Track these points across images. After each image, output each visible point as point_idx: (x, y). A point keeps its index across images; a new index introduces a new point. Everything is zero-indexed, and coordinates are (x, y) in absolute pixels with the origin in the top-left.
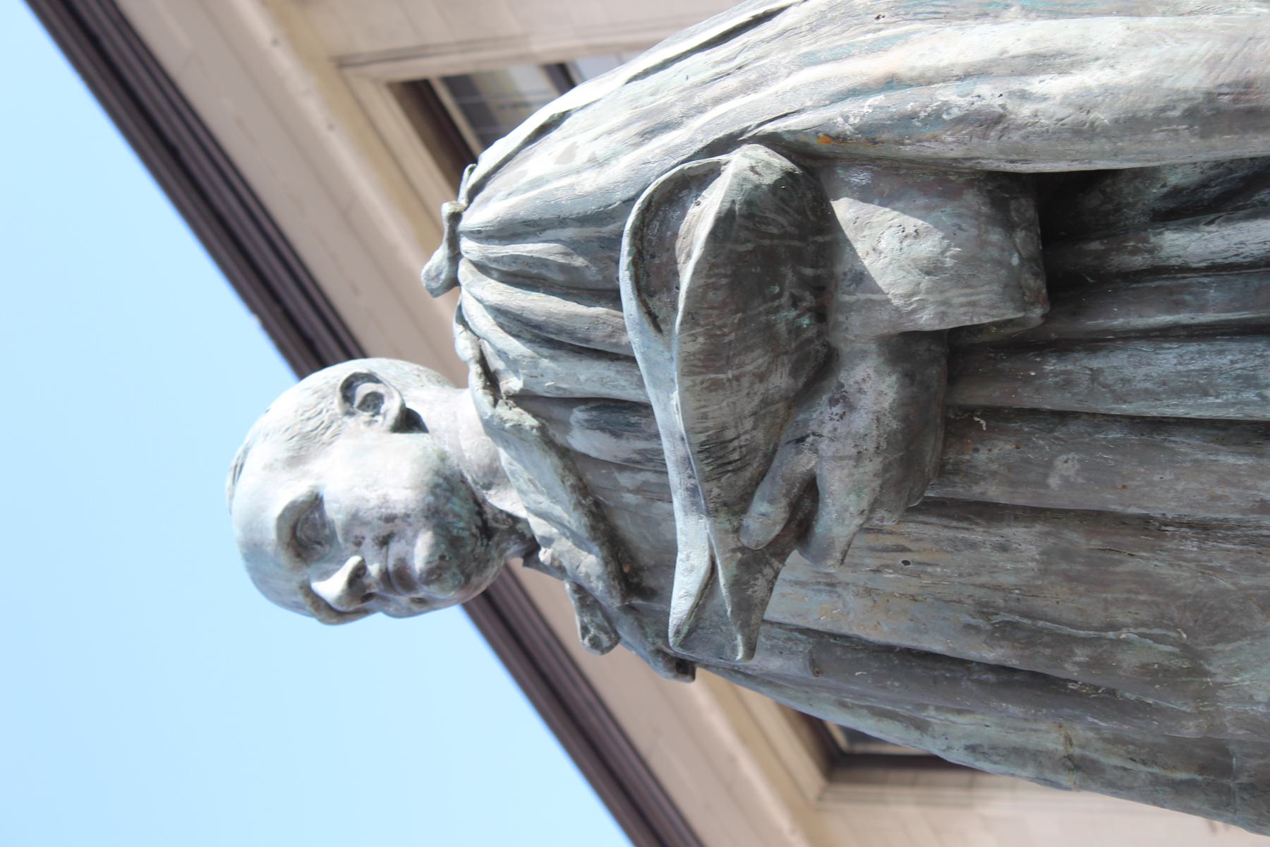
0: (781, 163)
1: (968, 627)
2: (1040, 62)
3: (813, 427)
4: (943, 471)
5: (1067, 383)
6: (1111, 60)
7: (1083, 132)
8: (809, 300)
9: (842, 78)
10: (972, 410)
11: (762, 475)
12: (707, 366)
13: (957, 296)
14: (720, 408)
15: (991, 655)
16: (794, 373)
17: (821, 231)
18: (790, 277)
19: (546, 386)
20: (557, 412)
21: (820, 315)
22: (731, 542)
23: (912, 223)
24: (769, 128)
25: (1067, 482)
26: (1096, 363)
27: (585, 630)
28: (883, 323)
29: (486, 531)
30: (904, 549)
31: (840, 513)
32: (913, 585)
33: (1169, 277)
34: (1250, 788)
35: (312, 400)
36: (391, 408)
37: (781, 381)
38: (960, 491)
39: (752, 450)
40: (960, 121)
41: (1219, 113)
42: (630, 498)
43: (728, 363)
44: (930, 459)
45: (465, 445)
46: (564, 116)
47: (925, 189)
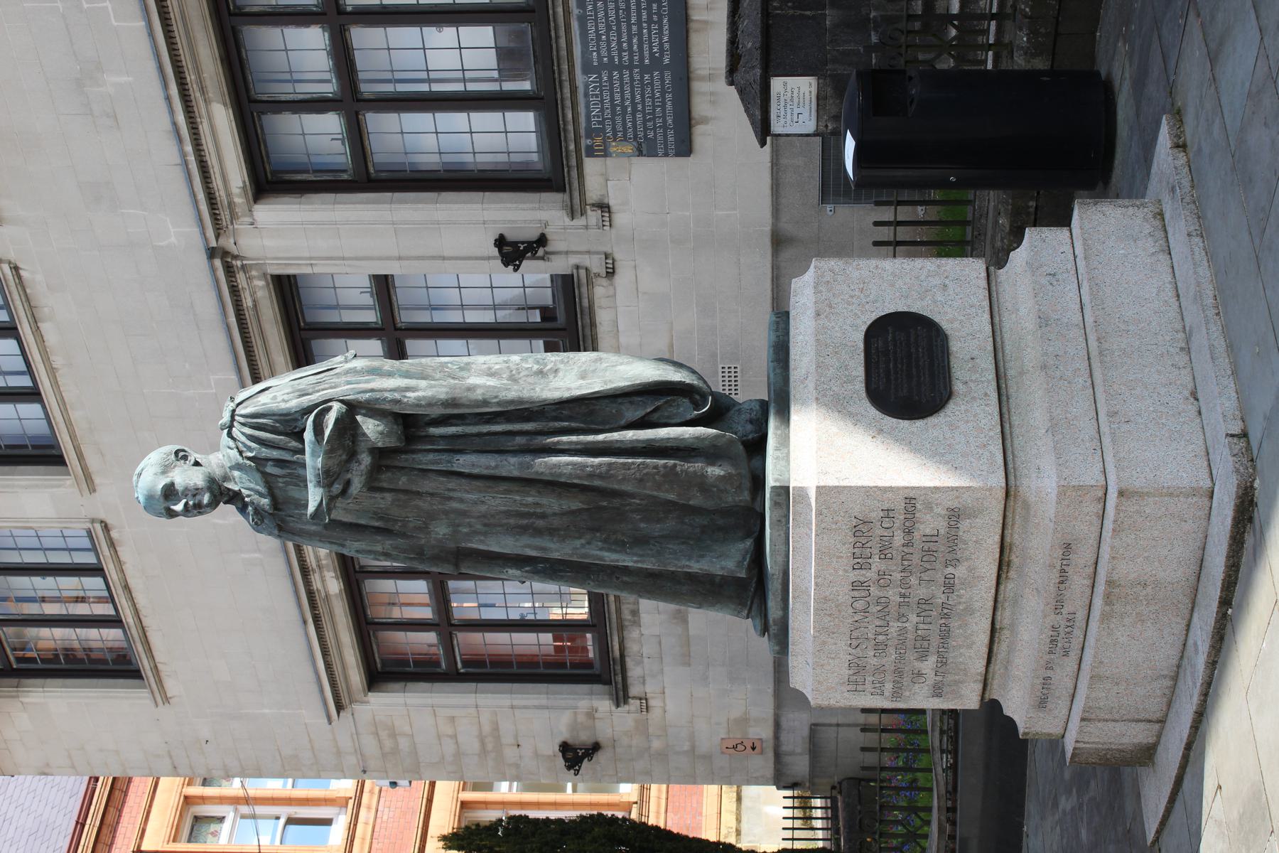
2: (408, 389)
6: (424, 390)
7: (418, 406)
12: (329, 453)
13: (387, 440)
14: (330, 463)
15: (377, 524)
29: (221, 494)
32: (357, 507)
33: (432, 439)
36: (192, 459)
37: (344, 457)
38: (376, 484)
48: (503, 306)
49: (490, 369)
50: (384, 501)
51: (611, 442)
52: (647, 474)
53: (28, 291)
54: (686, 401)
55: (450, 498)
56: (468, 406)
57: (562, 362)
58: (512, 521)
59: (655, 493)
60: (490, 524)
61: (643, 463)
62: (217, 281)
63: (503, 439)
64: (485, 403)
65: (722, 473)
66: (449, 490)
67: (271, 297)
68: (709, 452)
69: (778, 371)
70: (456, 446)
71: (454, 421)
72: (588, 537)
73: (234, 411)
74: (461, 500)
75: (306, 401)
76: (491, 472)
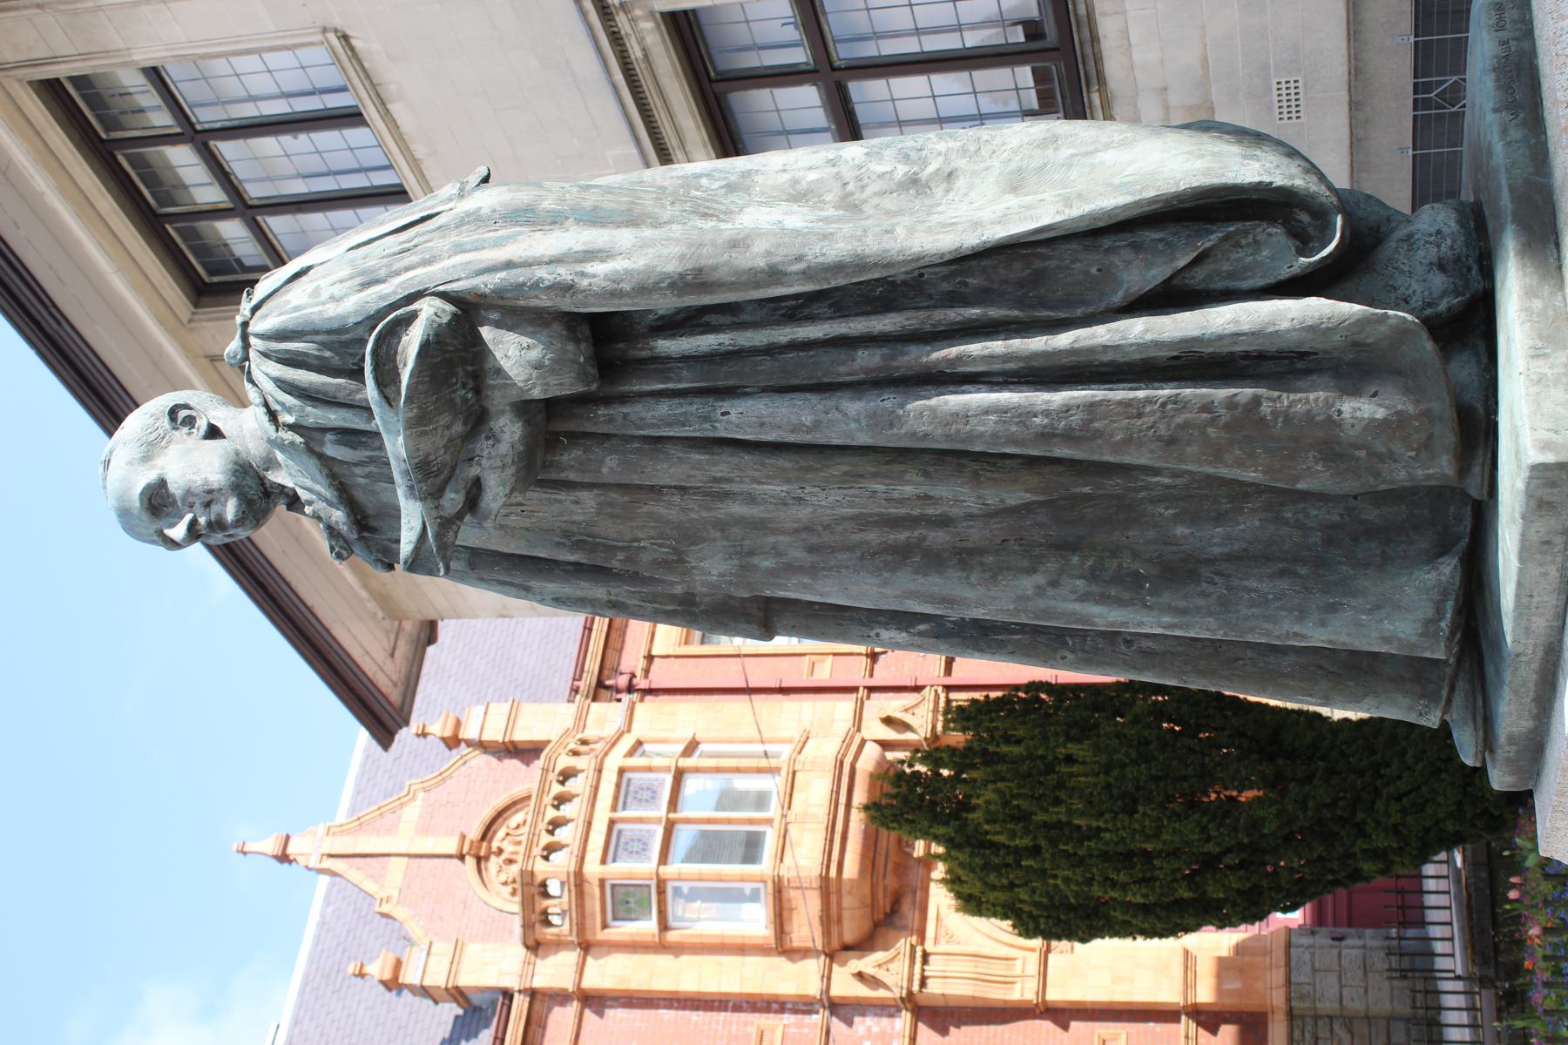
0: (450, 308)
1: (558, 544)
2: (590, 255)
3: (478, 452)
4: (546, 466)
5: (611, 420)
6: (627, 255)
7: (615, 294)
8: (471, 383)
9: (481, 261)
10: (558, 434)
11: (450, 478)
12: (418, 424)
13: (553, 380)
14: (426, 445)
15: (571, 558)
16: (465, 423)
17: (474, 345)
20: (316, 435)
21: (478, 391)
22: (434, 513)
23: (526, 340)
24: (441, 288)
26: (626, 410)
27: (332, 549)
28: (513, 396)
31: (495, 494)
32: (527, 523)
33: (662, 365)
36: (202, 424)
37: (458, 428)
38: (554, 476)
39: (444, 465)
40: (549, 288)
41: (687, 284)
44: (539, 463)
45: (250, 446)
46: (309, 268)
47: (531, 322)
48: (974, 26)
51: (1091, 350)
52: (1185, 426)
53: (366, 65)
54: (1277, 231)
55: (727, 495)
57: (963, 151)
58: (873, 537)
59: (1210, 470)
60: (823, 548)
61: (1174, 400)
62: (590, 28)
63: (824, 357)
64: (774, 274)
65: (1380, 413)
66: (715, 480)
67: (664, 42)
68: (1348, 363)
69: (1515, 134)
70: (720, 379)
71: (713, 319)
72: (1052, 566)
74: (751, 499)
75: (375, 297)
76: (806, 438)
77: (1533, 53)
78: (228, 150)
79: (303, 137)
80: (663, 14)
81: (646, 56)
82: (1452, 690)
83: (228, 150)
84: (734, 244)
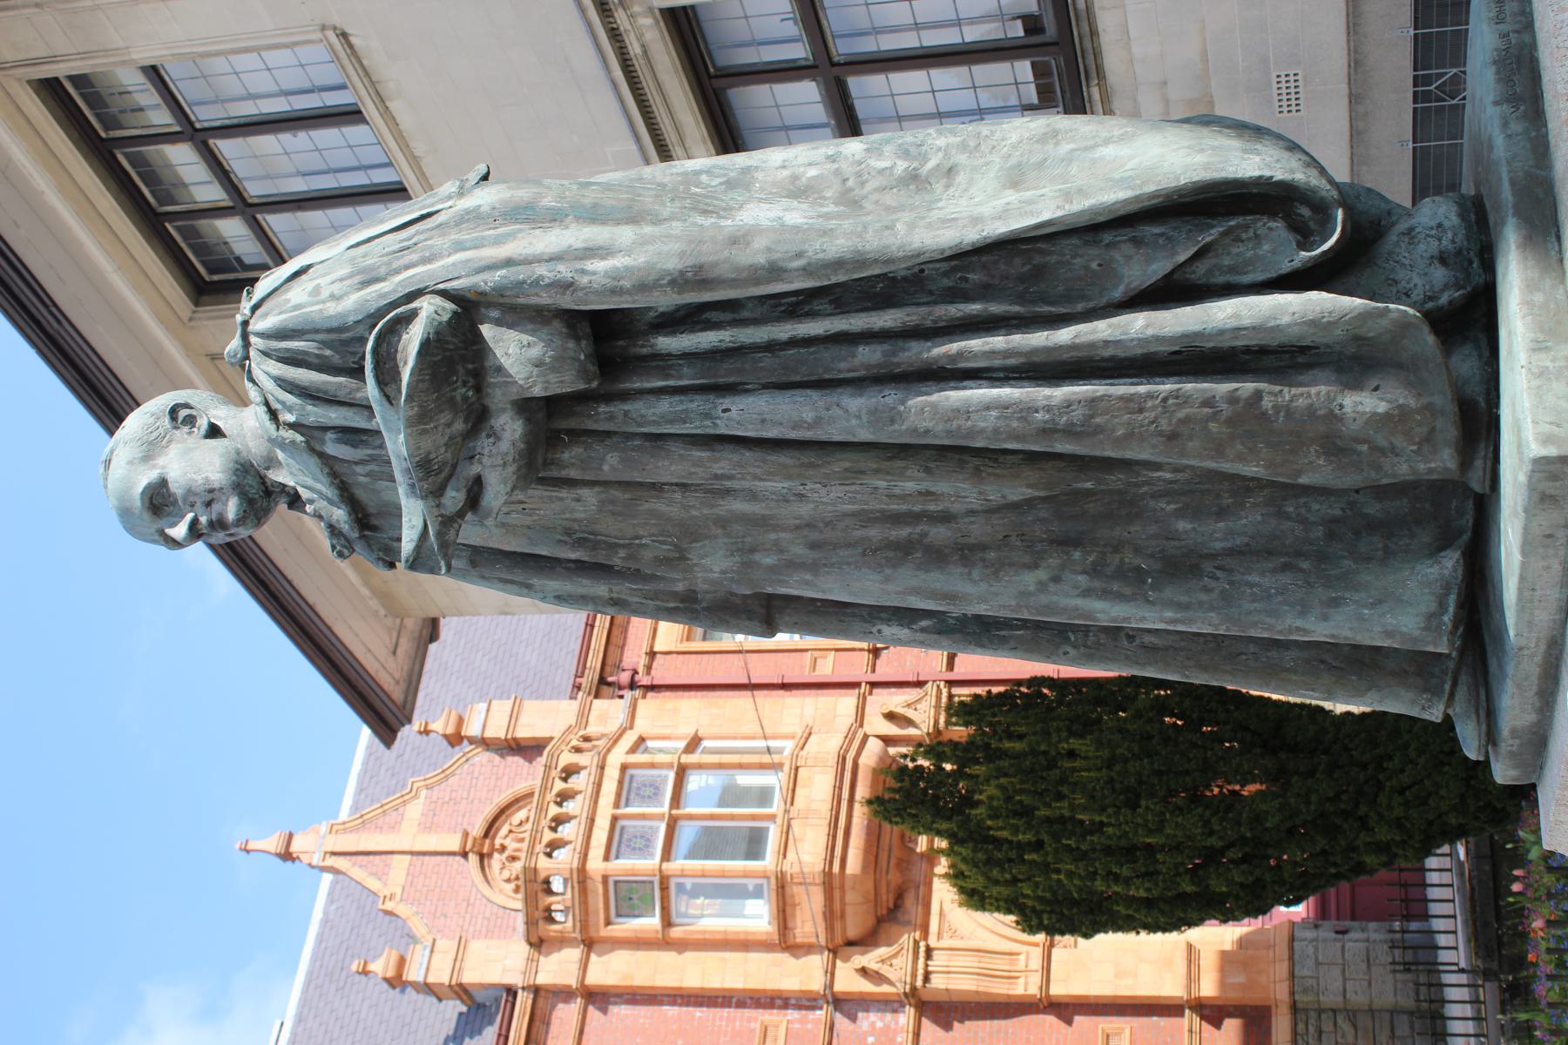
0: (450, 306)
1: (560, 541)
2: (591, 252)
3: (479, 450)
4: (547, 464)
5: (611, 418)
6: (628, 252)
7: (616, 291)
8: (471, 382)
9: (481, 259)
10: (559, 431)
12: (420, 421)
13: (553, 378)
14: (427, 443)
15: (573, 556)
16: (465, 421)
18: (461, 371)
19: (311, 420)
20: (316, 433)
21: (478, 389)
23: (526, 338)
24: (441, 286)
25: (613, 467)
27: (333, 547)
28: (514, 394)
30: (522, 502)
31: (496, 493)
32: (528, 521)
33: (662, 362)
34: (707, 609)
35: (151, 420)
36: (203, 424)
37: (459, 426)
38: (555, 473)
39: (445, 463)
40: (549, 285)
41: (687, 282)
42: (362, 479)
43: (431, 420)
44: (540, 460)
45: (251, 444)
46: (309, 267)
47: (532, 320)
49: (795, 178)
50: (584, 505)
52: (1187, 420)
53: (365, 62)
54: (1278, 225)
55: (728, 492)
56: (733, 283)
57: (963, 147)
58: (875, 533)
59: (1210, 464)
60: (824, 543)
61: (1176, 395)
62: (589, 25)
63: (826, 354)
64: (775, 271)
65: (1382, 407)
66: (716, 477)
67: (663, 38)
68: (1351, 358)
69: (1516, 127)
70: (722, 376)
71: (714, 316)
72: (1054, 561)
73: (245, 323)
74: (753, 496)
77: (1533, 45)
78: (226, 148)
79: (302, 135)
80: (661, 10)
81: (645, 52)
82: (1455, 684)
83: (226, 148)
84: (734, 241)
